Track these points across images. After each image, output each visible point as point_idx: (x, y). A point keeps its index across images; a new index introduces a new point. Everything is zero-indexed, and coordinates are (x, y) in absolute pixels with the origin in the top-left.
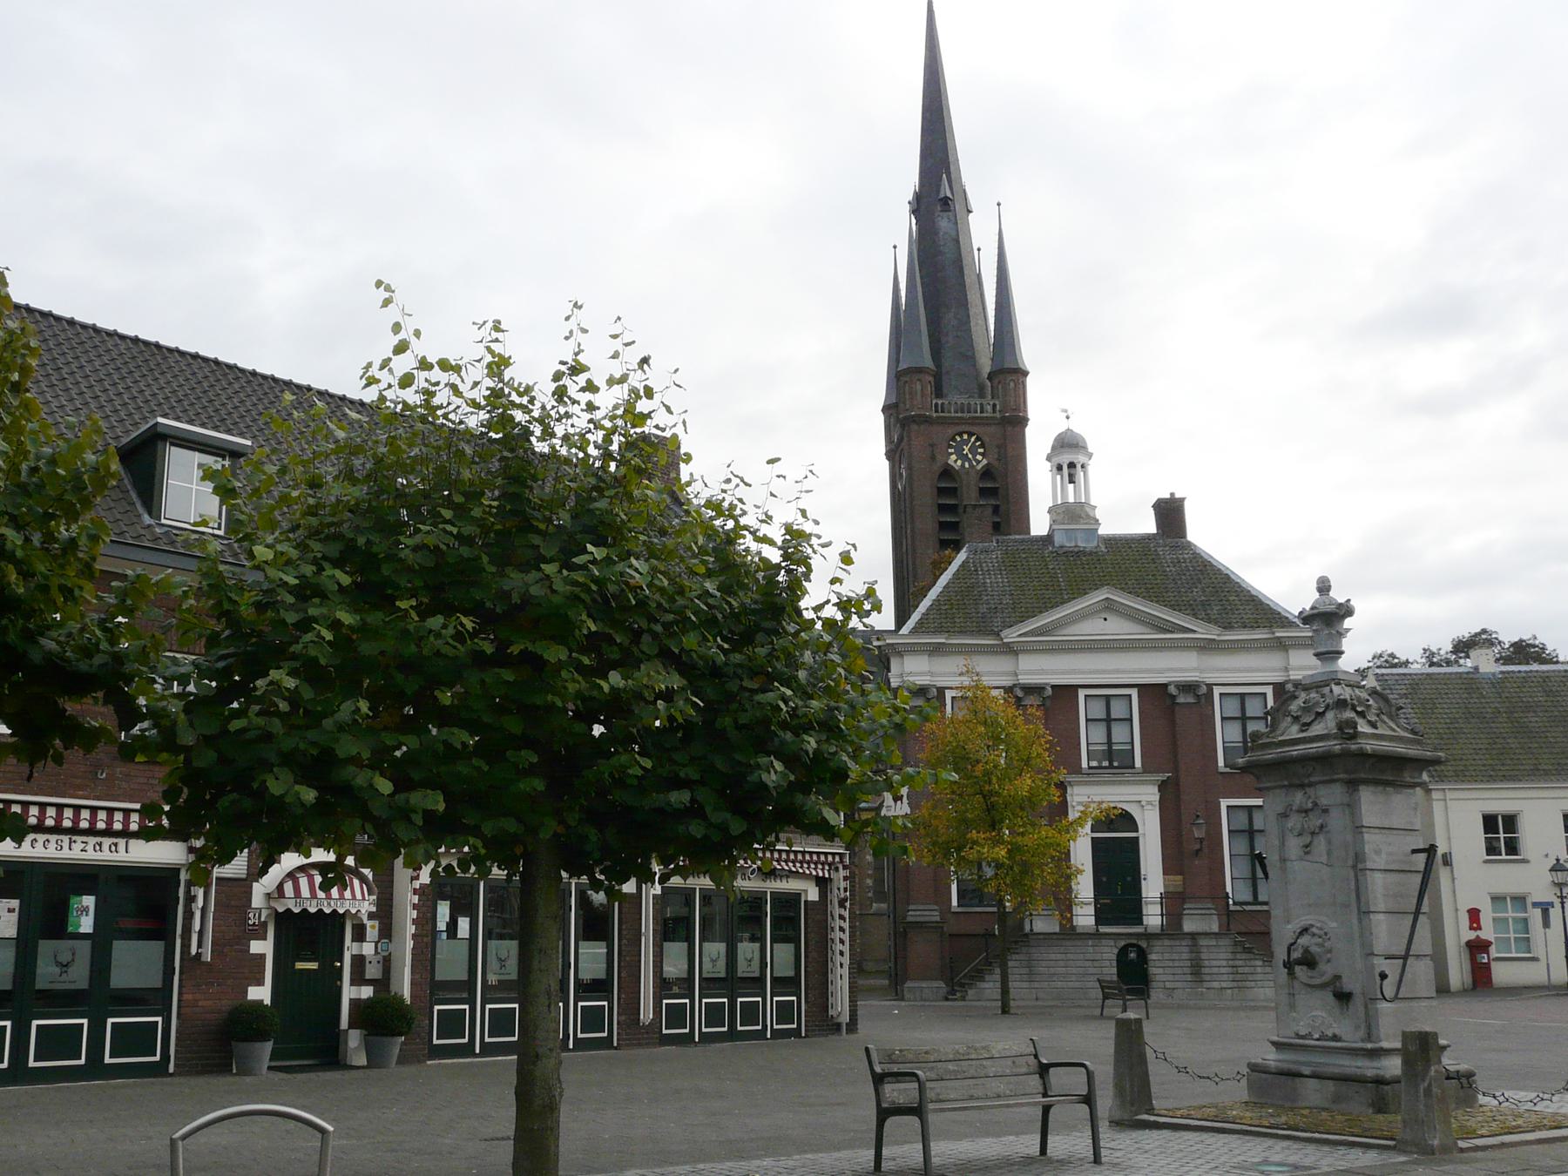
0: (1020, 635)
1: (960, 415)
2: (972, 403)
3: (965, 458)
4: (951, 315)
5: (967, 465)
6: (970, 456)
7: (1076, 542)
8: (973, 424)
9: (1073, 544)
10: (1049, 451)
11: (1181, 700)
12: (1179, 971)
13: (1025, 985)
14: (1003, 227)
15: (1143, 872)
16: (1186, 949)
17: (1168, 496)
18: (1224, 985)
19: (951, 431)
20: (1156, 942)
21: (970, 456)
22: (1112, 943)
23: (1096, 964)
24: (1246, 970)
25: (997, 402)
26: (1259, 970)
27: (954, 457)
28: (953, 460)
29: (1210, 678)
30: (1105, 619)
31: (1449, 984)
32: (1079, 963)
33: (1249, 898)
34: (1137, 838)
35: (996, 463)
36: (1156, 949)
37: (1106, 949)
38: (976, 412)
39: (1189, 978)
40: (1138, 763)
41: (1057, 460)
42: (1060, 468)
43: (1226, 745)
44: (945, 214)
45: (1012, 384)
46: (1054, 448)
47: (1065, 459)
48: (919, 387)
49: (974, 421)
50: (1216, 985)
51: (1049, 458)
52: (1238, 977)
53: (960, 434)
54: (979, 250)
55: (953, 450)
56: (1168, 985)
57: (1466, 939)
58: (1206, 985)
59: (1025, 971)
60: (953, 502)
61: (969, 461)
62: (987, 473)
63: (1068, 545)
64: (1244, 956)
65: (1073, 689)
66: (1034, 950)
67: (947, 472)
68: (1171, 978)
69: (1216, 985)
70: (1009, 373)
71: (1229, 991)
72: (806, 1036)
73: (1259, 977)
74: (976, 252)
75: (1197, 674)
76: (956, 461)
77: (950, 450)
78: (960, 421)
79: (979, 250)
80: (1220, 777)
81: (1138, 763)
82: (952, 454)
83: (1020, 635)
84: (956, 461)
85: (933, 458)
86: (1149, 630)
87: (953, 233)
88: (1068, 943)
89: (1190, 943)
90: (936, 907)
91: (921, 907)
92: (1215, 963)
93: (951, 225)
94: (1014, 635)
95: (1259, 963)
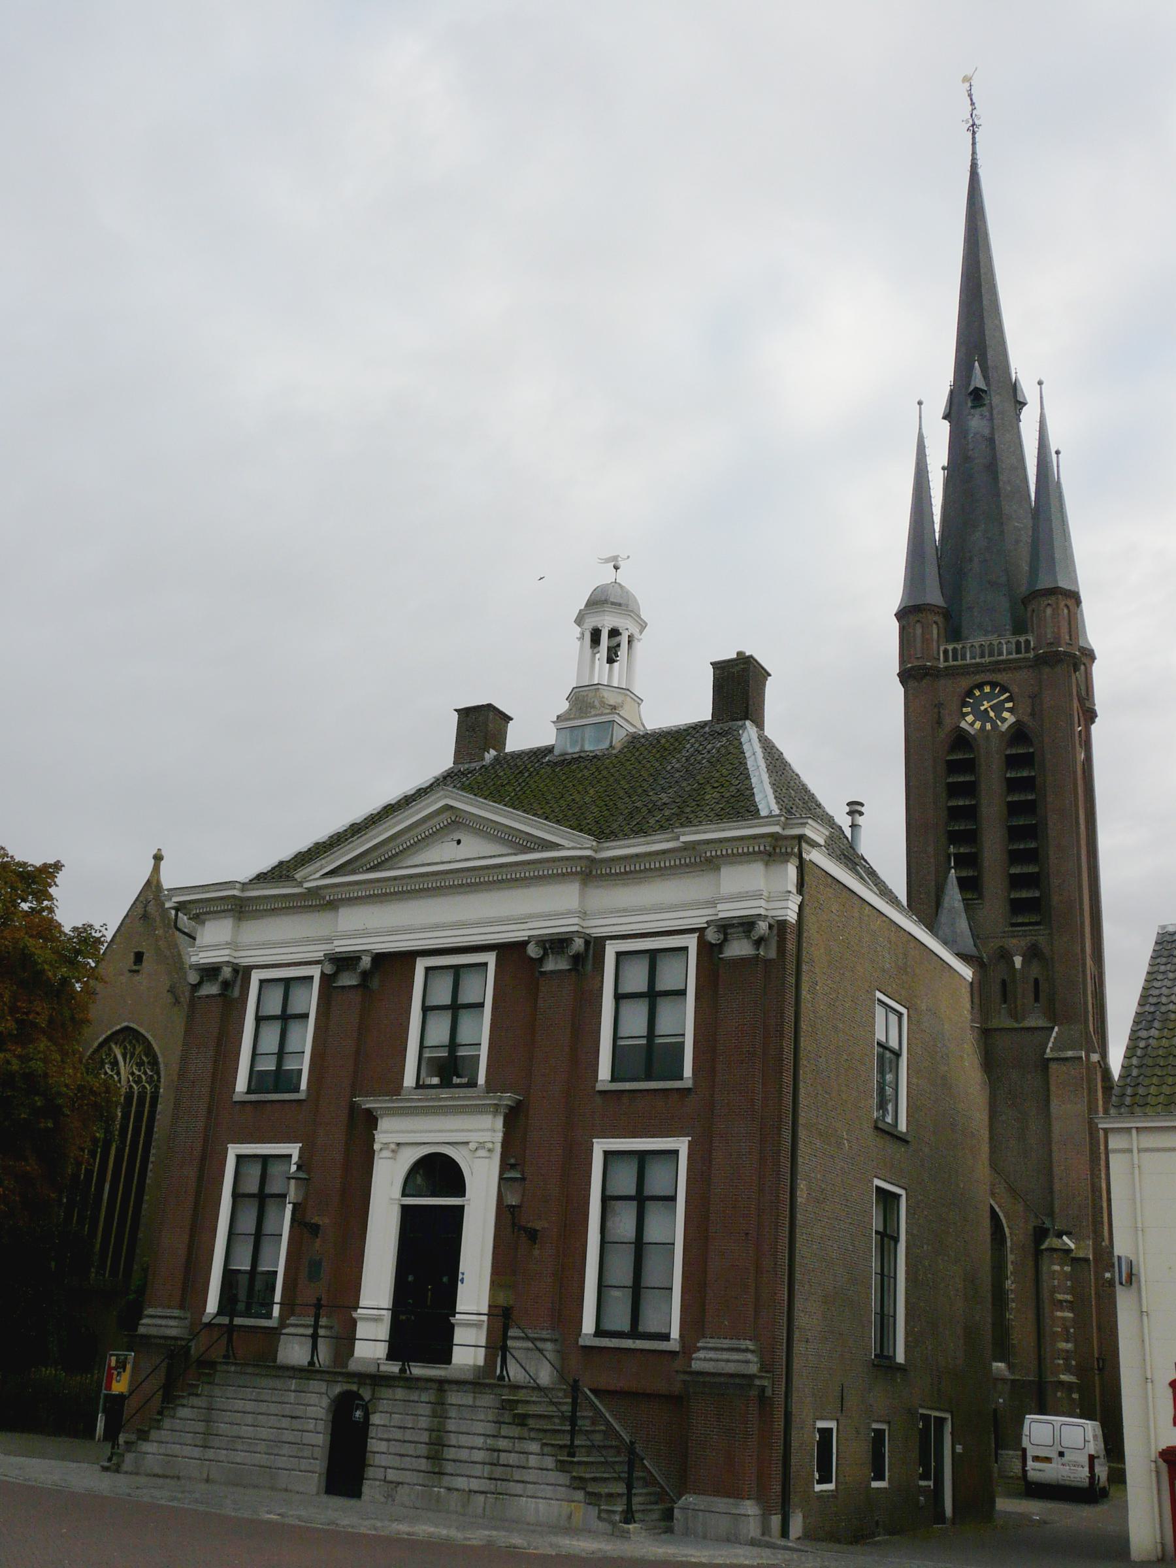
0: (332, 873)
1: (978, 660)
2: (995, 643)
3: (983, 716)
4: (978, 534)
5: (988, 726)
6: (992, 714)
7: (582, 746)
8: (993, 671)
9: (577, 750)
10: (583, 608)
11: (550, 965)
12: (409, 1449)
13: (197, 1452)
14: (1046, 411)
15: (461, 1270)
16: (426, 1410)
17: (735, 656)
18: (475, 1484)
19: (965, 683)
20: (386, 1393)
21: (992, 714)
22: (323, 1387)
23: (296, 1424)
24: (512, 1459)
25: (1030, 638)
26: (533, 1461)
27: (970, 718)
28: (970, 723)
29: (598, 927)
30: (459, 842)
31: (1127, 1540)
32: (273, 1421)
33: (626, 1327)
34: (461, 1208)
35: (1026, 719)
36: (384, 1405)
37: (313, 1398)
38: (1000, 654)
39: (423, 1464)
40: (481, 1080)
41: (591, 622)
42: (596, 636)
43: (621, 1043)
44: (978, 411)
45: (1049, 611)
46: (587, 605)
47: (607, 622)
48: (919, 631)
49: (997, 667)
50: (461, 1483)
51: (579, 621)
52: (499, 1472)
53: (980, 686)
54: (1058, 453)
55: (969, 709)
56: (392, 1475)
57: (1163, 1446)
58: (447, 1481)
59: (200, 1427)
60: (968, 778)
61: (990, 720)
62: (1019, 734)
63: (570, 751)
64: (515, 1431)
65: (409, 957)
66: (217, 1391)
67: (962, 740)
68: (396, 1462)
69: (461, 1483)
70: (1044, 595)
71: (481, 1498)
72: (954, 1522)
73: (530, 1476)
74: (1054, 456)
75: (576, 921)
76: (972, 724)
77: (965, 710)
78: (979, 668)
79: (1058, 453)
80: (598, 1100)
81: (481, 1080)
82: (968, 714)
83: (332, 873)
84: (972, 724)
85: (939, 722)
86: (505, 850)
87: (986, 432)
88: (264, 1382)
89: (433, 1399)
90: (749, 1344)
91: (727, 1343)
92: (464, 1440)
93: (985, 423)
94: (318, 875)
95: (534, 1447)
